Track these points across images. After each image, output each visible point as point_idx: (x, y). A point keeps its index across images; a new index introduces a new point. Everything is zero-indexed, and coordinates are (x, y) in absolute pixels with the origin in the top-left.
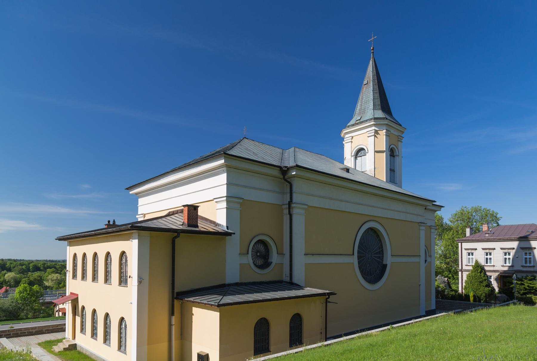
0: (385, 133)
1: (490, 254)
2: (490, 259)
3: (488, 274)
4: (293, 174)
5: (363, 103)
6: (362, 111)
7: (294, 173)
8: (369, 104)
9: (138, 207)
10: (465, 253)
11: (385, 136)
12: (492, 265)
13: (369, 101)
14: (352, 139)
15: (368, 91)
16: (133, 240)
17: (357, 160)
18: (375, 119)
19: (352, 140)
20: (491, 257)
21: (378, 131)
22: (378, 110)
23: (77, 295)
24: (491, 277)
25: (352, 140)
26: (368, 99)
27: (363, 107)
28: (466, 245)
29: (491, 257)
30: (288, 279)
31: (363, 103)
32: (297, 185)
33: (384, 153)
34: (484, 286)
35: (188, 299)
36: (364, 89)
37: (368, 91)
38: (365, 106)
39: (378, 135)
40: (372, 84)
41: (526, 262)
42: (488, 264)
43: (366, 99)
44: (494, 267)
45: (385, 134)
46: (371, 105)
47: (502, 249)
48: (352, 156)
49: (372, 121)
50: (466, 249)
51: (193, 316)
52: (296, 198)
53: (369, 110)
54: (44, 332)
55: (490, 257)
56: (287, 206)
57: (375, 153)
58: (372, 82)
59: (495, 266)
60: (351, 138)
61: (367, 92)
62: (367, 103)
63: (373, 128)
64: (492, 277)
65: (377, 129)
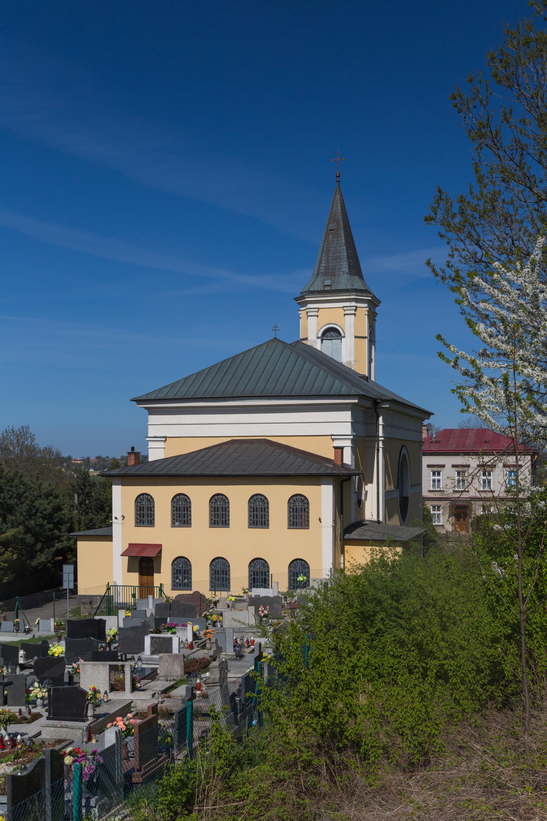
1: (439, 474)
2: (439, 481)
5: (331, 258)
8: (342, 263)
11: (367, 317)
19: (356, 312)
20: (432, 478)
26: (338, 254)
27: (330, 265)
28: (426, 460)
29: (491, 478)
36: (330, 236)
38: (335, 264)
41: (434, 486)
43: (336, 255)
45: (366, 313)
46: (344, 266)
47: (453, 466)
50: (429, 466)
54: (492, 503)
55: (439, 478)
60: (354, 308)
62: (338, 261)
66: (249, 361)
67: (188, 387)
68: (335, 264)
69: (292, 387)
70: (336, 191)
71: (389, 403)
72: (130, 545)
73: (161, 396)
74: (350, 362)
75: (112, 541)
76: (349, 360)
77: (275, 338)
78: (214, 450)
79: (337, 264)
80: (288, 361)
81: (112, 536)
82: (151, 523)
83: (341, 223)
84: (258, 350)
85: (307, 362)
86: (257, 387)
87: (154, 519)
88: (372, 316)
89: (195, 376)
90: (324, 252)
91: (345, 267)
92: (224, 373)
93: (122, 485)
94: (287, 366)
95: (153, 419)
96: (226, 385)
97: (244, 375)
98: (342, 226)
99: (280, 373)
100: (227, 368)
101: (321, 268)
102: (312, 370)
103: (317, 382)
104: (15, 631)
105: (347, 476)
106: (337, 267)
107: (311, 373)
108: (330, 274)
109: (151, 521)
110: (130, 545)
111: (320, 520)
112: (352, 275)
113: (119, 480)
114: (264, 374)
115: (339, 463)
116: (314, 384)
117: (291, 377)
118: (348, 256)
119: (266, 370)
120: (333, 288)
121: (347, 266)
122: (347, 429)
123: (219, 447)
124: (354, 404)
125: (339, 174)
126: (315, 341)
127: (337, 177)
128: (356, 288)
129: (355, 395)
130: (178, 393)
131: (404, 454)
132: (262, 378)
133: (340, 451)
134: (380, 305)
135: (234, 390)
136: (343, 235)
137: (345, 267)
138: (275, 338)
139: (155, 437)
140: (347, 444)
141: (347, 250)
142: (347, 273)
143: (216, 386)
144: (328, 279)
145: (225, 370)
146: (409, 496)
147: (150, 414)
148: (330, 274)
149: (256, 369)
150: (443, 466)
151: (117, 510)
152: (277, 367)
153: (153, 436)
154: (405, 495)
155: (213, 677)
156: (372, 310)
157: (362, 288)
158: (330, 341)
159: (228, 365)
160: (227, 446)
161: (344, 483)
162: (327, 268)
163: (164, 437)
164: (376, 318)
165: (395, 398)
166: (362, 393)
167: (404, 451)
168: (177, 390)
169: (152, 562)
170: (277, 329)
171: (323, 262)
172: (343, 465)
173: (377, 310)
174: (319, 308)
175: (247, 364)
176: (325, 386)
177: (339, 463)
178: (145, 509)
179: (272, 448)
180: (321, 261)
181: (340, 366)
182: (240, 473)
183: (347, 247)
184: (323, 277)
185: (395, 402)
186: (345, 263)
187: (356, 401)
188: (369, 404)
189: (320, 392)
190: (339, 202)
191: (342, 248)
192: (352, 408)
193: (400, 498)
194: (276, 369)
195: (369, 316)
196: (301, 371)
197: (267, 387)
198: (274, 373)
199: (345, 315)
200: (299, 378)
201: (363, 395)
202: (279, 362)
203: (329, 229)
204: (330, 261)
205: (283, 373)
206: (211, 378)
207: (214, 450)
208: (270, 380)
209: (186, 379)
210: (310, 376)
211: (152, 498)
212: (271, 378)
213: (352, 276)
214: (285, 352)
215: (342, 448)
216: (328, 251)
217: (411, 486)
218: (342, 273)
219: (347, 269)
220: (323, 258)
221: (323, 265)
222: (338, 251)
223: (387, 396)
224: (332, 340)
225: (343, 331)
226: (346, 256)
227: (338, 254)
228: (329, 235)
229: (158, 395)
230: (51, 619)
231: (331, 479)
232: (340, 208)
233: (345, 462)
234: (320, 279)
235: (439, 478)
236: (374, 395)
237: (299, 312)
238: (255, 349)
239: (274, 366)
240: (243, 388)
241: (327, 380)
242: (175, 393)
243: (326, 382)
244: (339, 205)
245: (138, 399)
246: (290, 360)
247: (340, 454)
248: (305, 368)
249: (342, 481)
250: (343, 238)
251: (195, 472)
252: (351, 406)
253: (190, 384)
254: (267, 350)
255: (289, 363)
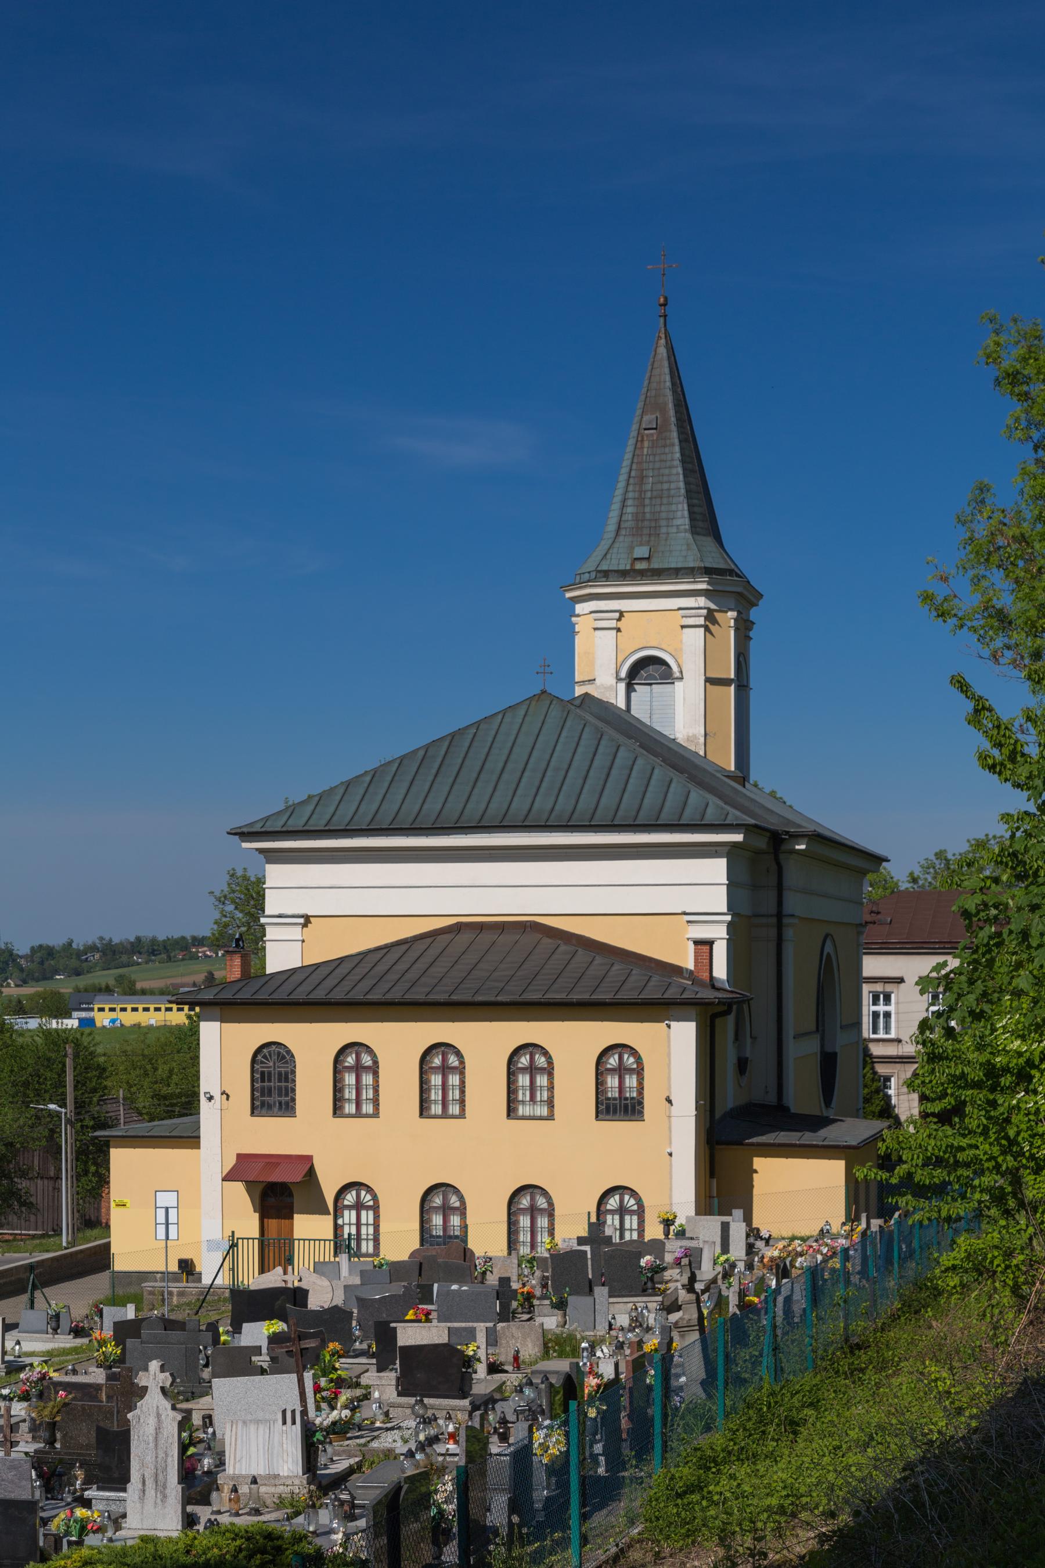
0: (732, 621)
1: (887, 999)
2: (887, 1015)
3: (882, 1069)
4: (797, 847)
5: (649, 494)
6: (646, 523)
7: (803, 847)
8: (674, 507)
9: (264, 889)
10: (866, 998)
12: (893, 1035)
13: (668, 497)
14: (619, 620)
15: (663, 457)
16: (673, 1024)
17: (633, 694)
18: (708, 571)
19: (620, 625)
20: (891, 1008)
21: (715, 614)
22: (704, 535)
23: (309, 1158)
24: (890, 1080)
25: (620, 625)
27: (647, 509)
29: (891, 1008)
30: (772, 1099)
31: (649, 494)
32: (793, 875)
33: (730, 686)
34: (874, 1112)
35: (750, 1141)
36: (646, 444)
37: (663, 457)
39: (714, 625)
40: (675, 434)
42: (881, 1035)
43: (659, 486)
44: (900, 1045)
46: (679, 514)
48: (619, 679)
49: (704, 581)
51: (755, 1175)
52: (793, 903)
53: (674, 530)
55: (887, 1008)
56: (774, 920)
57: (708, 684)
58: (674, 428)
59: (903, 1042)
60: (617, 615)
61: (657, 458)
62: (665, 501)
63: (702, 601)
64: (893, 1079)
65: (713, 606)
66: (489, 744)
67: (356, 803)
68: (658, 509)
69: (593, 806)
70: (659, 337)
71: (806, 840)
72: (240, 1156)
73: (297, 822)
74: (695, 736)
75: (199, 1148)
76: (691, 732)
77: (544, 692)
78: (421, 946)
79: (663, 508)
80: (578, 744)
81: (199, 1137)
82: (287, 1108)
83: (672, 412)
84: (507, 719)
85: (622, 749)
86: (514, 805)
87: (294, 1100)
88: (744, 629)
89: (368, 778)
90: (632, 481)
91: (683, 517)
92: (434, 771)
93: (222, 1022)
94: (576, 757)
95: (276, 875)
96: (442, 800)
97: (482, 776)
98: (673, 419)
99: (563, 773)
100: (439, 760)
101: (624, 518)
102: (636, 767)
103: (648, 795)
104: (50, 1330)
105: (724, 1004)
106: (664, 515)
107: (634, 774)
108: (646, 531)
109: (287, 1104)
110: (240, 1156)
111: (669, 1101)
112: (698, 534)
113: (217, 1010)
114: (526, 774)
115: (705, 975)
116: (643, 799)
117: (589, 782)
118: (688, 491)
119: (530, 766)
120: (655, 565)
121: (686, 513)
122: (718, 900)
123: (430, 940)
124: (734, 845)
125: (666, 299)
126: (610, 688)
127: (661, 305)
128: (708, 565)
129: (737, 825)
130: (335, 818)
131: (829, 954)
132: (522, 784)
133: (706, 948)
134: (761, 602)
135: (483, 815)
136: (676, 441)
137: (681, 515)
138: (544, 692)
139: (280, 916)
140: (719, 932)
141: (685, 476)
142: (686, 531)
143: (420, 801)
144: (641, 545)
145: (436, 765)
146: (837, 1050)
147: (269, 862)
148: (646, 531)
149: (506, 762)
150: (900, 980)
151: (209, 1080)
152: (554, 759)
153: (277, 913)
154: (829, 1049)
155: (687, 1317)
156: (744, 616)
157: (722, 566)
158: (648, 687)
159: (443, 752)
160: (447, 937)
161: (718, 1021)
162: (638, 518)
163: (302, 916)
164: (751, 634)
165: (820, 830)
166: (752, 821)
167: (829, 948)
168: (332, 809)
169: (291, 1195)
170: (548, 670)
171: (629, 502)
172: (712, 981)
173: (754, 614)
174: (621, 614)
175: (486, 750)
176: (668, 804)
177: (705, 975)
178: (275, 1078)
179: (550, 941)
180: (624, 500)
181: (671, 745)
182: (492, 998)
183: (684, 469)
184: (630, 539)
185: (819, 839)
186: (680, 507)
187: (738, 838)
188: (761, 843)
189: (657, 819)
190: (666, 364)
191: (674, 471)
192: (731, 852)
193: (821, 1053)
194: (552, 764)
195: (737, 630)
196: (610, 769)
197: (536, 806)
198: (549, 773)
199: (683, 627)
200: (608, 785)
201: (756, 826)
202: (558, 748)
203: (644, 426)
204: (647, 502)
205: (571, 773)
206: (406, 784)
207: (421, 946)
208: (542, 790)
209: (348, 785)
210: (631, 781)
211: (289, 1052)
212: (544, 785)
213: (698, 537)
214: (568, 724)
215: (710, 943)
216: (642, 478)
217: (841, 1028)
218: (674, 530)
219: (687, 521)
220: (630, 495)
221: (629, 510)
222: (665, 479)
223: (799, 826)
224: (650, 684)
225: (679, 666)
226: (683, 491)
227: (665, 486)
228: (642, 441)
229: (290, 822)
230: (129, 1305)
231: (693, 1011)
232: (668, 378)
233: (715, 974)
234: (623, 541)
235: (887, 1008)
236: (772, 823)
237: (574, 619)
238: (500, 716)
239: (547, 757)
240: (483, 806)
241: (672, 789)
242: (328, 817)
243: (670, 796)
244: (667, 370)
245: (245, 830)
246: (582, 743)
247: (706, 955)
248: (618, 761)
249: (714, 1017)
250: (677, 448)
251: (389, 997)
252: (726, 849)
253: (359, 797)
254: (528, 719)
255: (580, 750)
